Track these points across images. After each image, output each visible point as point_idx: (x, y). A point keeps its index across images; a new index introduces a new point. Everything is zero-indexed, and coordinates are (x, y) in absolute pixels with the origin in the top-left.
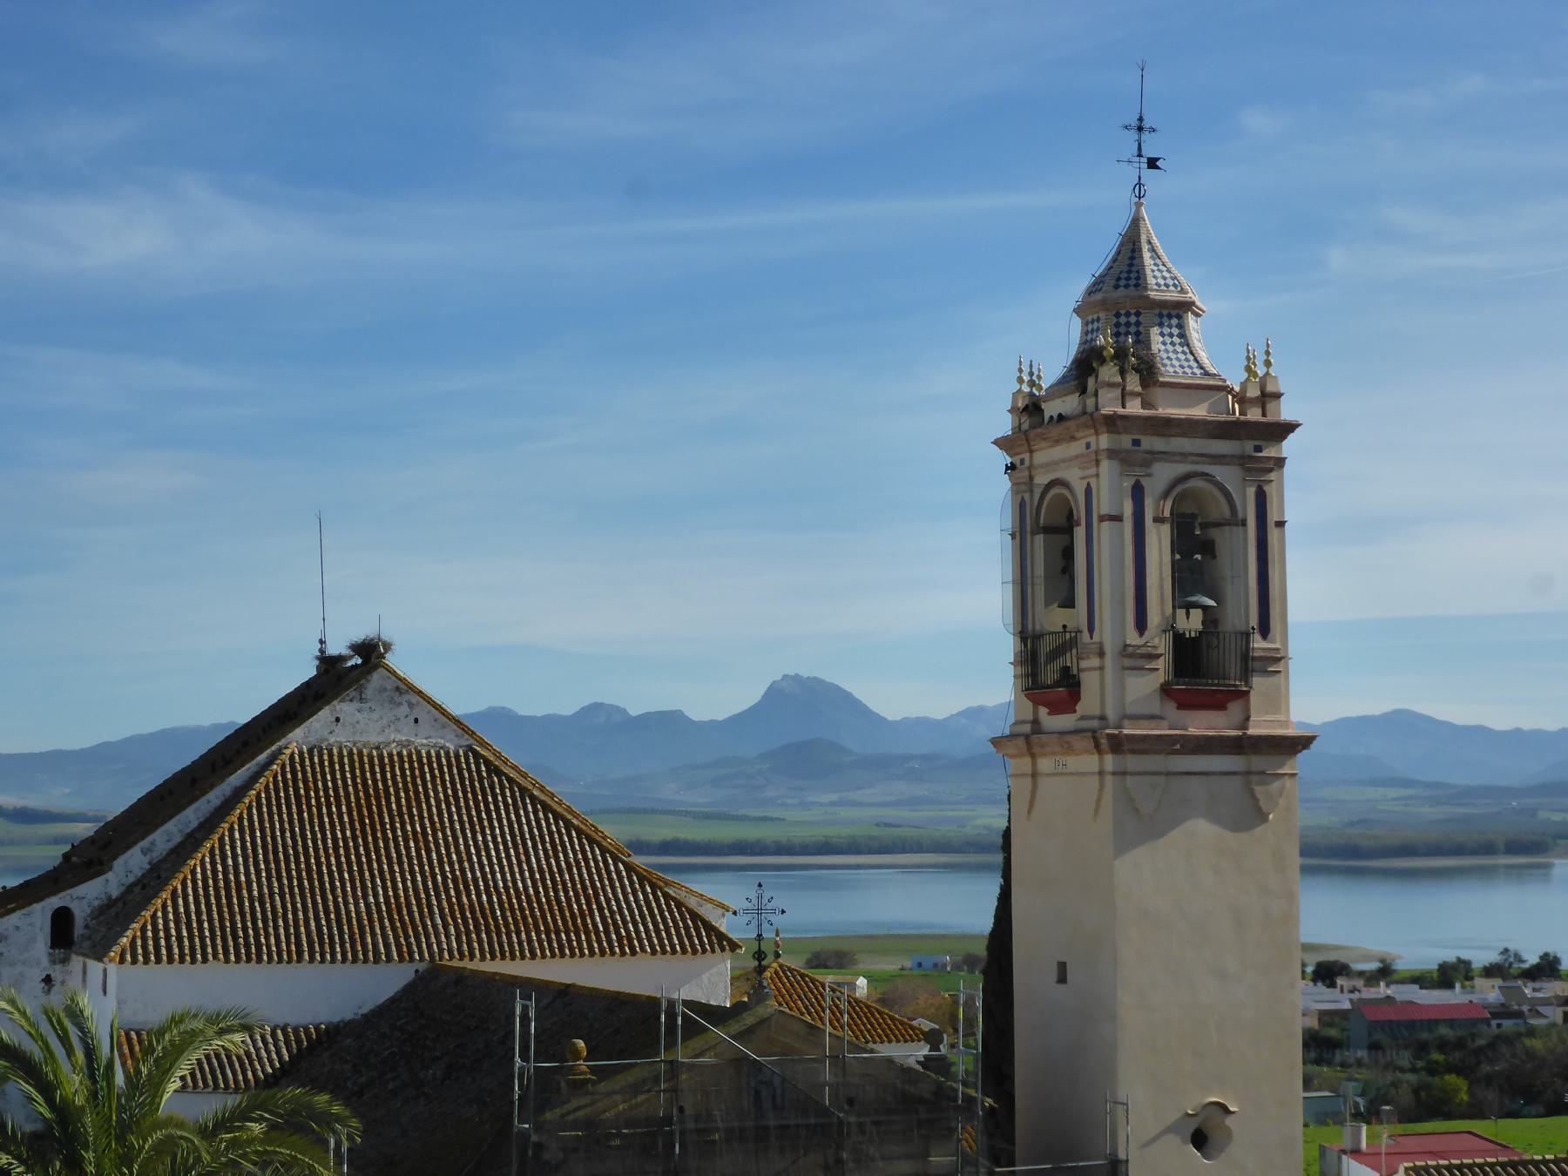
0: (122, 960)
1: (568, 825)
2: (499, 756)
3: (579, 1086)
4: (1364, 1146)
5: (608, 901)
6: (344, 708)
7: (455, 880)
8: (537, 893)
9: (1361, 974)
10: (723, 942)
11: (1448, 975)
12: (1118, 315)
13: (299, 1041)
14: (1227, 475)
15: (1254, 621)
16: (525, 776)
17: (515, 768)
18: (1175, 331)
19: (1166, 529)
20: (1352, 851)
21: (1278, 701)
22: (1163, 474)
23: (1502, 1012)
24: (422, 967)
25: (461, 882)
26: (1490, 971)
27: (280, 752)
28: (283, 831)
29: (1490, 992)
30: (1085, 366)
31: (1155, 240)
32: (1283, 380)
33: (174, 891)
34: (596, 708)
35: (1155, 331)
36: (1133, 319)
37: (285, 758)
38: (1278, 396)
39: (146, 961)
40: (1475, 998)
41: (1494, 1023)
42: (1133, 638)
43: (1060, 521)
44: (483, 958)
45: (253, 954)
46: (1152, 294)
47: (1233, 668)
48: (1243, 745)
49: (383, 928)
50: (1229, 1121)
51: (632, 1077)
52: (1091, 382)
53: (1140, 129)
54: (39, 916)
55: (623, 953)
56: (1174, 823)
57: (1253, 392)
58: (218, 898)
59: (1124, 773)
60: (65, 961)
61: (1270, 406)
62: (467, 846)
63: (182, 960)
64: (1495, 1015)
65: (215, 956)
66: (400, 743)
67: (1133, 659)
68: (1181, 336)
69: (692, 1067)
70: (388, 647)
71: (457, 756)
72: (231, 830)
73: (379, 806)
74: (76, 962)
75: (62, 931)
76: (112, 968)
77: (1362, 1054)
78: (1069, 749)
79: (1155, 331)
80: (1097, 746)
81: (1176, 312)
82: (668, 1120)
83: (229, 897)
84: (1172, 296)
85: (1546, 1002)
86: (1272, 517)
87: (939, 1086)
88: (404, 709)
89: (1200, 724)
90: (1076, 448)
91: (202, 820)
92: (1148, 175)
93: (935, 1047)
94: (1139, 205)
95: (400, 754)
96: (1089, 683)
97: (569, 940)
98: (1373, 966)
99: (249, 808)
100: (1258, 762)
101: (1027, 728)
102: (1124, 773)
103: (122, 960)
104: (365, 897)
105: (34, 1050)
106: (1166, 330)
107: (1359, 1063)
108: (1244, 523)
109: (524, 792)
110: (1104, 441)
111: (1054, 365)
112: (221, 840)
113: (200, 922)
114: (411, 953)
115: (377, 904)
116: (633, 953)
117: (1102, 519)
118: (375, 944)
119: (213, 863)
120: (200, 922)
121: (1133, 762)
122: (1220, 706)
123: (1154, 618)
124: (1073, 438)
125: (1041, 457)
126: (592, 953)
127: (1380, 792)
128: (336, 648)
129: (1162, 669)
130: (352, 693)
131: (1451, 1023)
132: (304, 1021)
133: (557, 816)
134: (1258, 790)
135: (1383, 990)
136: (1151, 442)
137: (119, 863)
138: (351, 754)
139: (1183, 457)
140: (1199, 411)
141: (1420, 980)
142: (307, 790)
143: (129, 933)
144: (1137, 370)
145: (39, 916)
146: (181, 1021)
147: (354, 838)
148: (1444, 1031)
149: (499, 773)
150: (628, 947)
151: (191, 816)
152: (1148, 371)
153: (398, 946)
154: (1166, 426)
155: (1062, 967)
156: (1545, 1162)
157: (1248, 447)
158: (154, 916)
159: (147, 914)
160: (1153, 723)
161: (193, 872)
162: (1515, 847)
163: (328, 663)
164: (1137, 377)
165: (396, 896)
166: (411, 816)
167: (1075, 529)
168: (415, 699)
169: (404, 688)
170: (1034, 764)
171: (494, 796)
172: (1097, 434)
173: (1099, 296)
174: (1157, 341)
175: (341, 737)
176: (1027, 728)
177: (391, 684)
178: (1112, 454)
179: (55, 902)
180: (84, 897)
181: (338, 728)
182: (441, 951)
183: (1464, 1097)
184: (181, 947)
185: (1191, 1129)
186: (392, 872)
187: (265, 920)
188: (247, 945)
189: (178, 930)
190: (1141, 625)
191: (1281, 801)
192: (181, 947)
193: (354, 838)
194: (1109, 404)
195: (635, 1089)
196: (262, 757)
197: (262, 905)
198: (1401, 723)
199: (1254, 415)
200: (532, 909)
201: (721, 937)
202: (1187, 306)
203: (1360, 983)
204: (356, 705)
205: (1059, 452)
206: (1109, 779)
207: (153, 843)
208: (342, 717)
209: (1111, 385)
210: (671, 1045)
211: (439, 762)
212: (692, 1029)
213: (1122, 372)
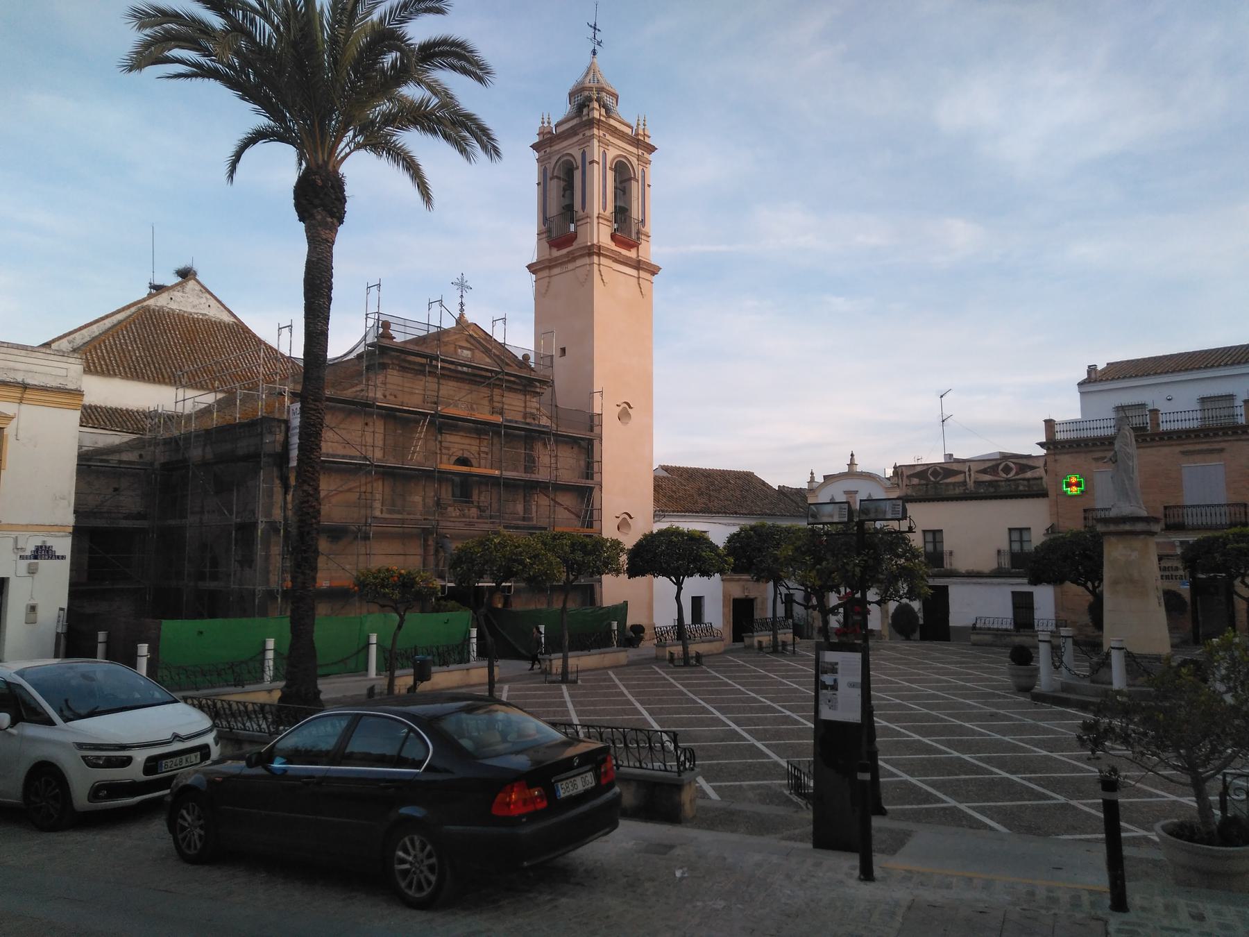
88: (204, 300)
91: (101, 332)
92: (597, 47)
146: (463, 140)
167: (575, 171)
175: (174, 306)
190: (605, 209)
204: (180, 294)
207: (74, 339)
208: (173, 297)
211: (227, 326)
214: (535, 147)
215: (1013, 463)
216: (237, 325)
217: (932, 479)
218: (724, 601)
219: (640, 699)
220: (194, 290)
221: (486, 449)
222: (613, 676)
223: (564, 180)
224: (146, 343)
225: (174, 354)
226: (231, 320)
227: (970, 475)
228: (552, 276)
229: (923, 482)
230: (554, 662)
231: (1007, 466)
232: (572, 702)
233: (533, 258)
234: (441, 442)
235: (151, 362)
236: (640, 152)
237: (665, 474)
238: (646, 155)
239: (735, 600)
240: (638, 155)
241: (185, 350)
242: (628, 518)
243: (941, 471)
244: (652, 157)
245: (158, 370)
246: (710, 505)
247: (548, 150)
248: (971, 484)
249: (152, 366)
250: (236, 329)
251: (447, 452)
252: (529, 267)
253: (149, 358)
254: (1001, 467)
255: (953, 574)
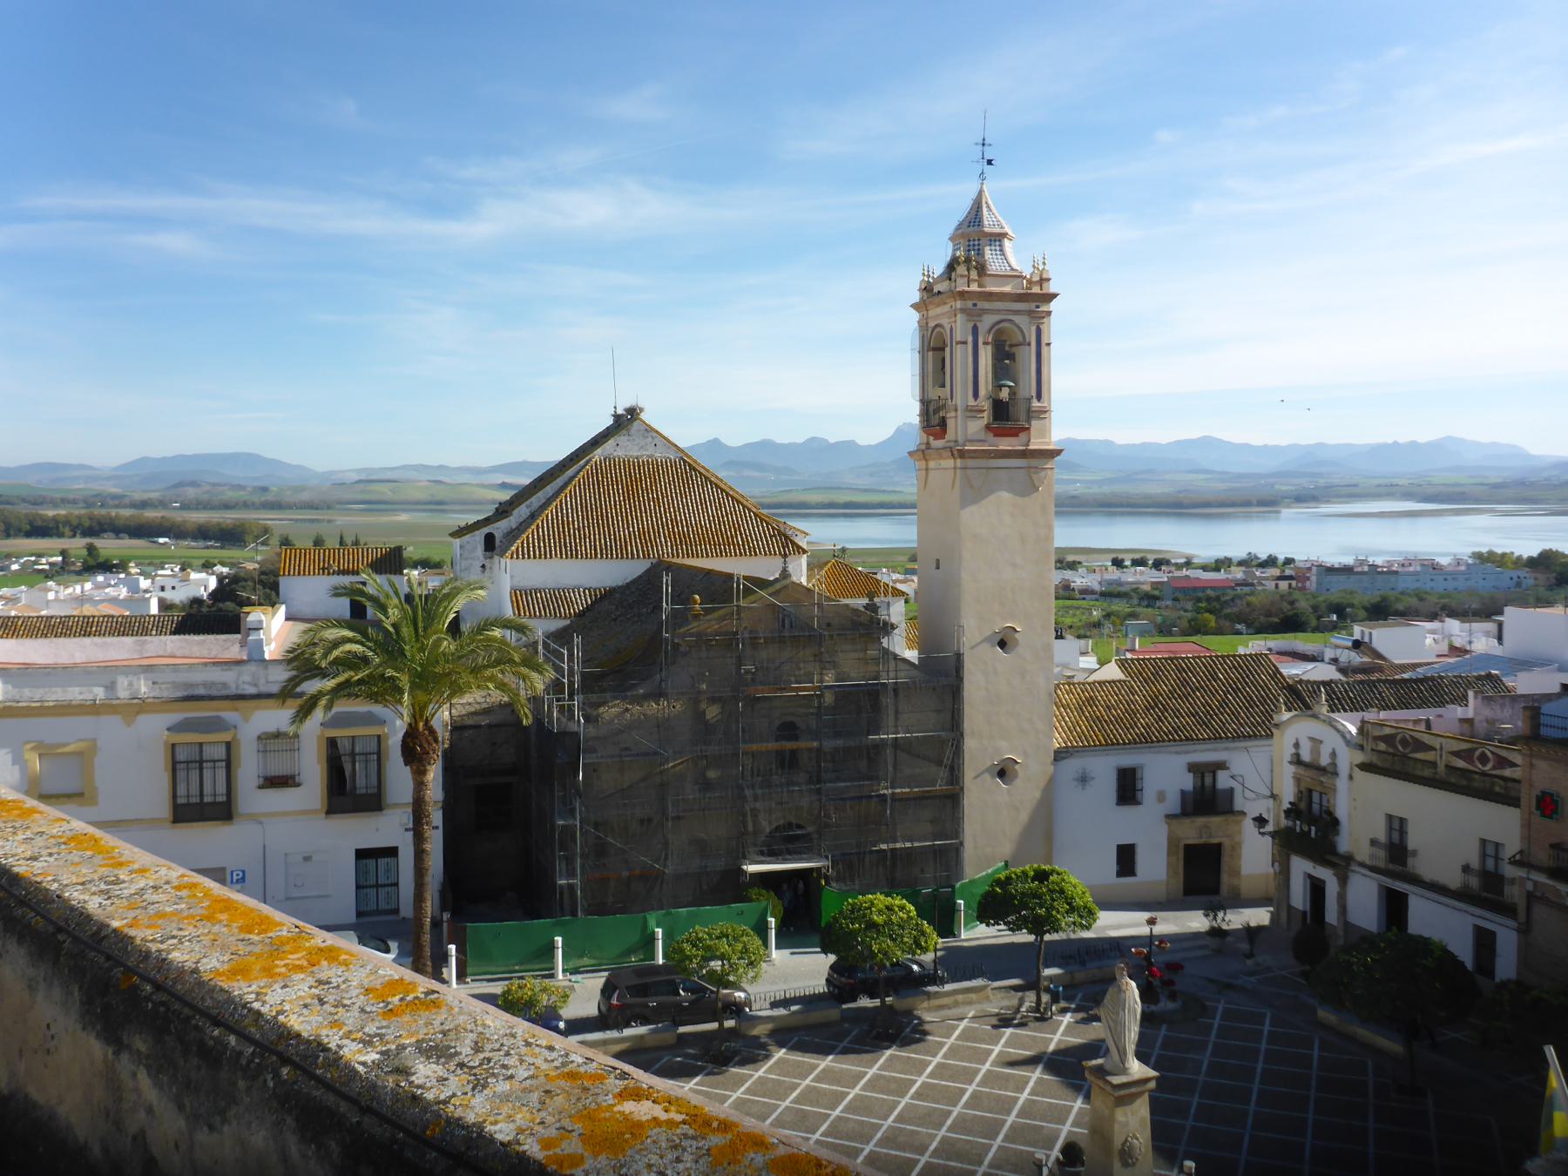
0: (512, 558)
1: (727, 494)
2: (695, 462)
3: (696, 617)
4: (1137, 647)
5: (745, 530)
6: (622, 439)
7: (672, 521)
8: (711, 527)
9: (1176, 564)
10: (805, 552)
11: (1220, 564)
12: (969, 241)
13: (596, 595)
14: (1021, 320)
15: (1034, 393)
16: (708, 471)
17: (703, 467)
18: (998, 248)
19: (989, 348)
20: (1109, 505)
21: (1045, 432)
22: (987, 321)
23: (1244, 583)
24: (654, 561)
25: (675, 522)
26: (1241, 563)
27: (590, 460)
28: (590, 497)
29: (1238, 574)
30: (951, 267)
31: (990, 202)
32: (1052, 271)
33: (538, 525)
34: (813, 439)
35: (987, 248)
36: (976, 243)
37: (593, 462)
38: (1049, 280)
39: (523, 558)
40: (1230, 577)
41: (1238, 588)
42: (971, 402)
43: (940, 345)
44: (683, 557)
45: (573, 554)
46: (986, 229)
47: (1023, 416)
48: (1025, 454)
49: (636, 543)
50: (1017, 635)
51: (721, 612)
52: (953, 274)
53: (983, 145)
54: (479, 536)
55: (751, 555)
56: (991, 492)
57: (1036, 278)
58: (558, 528)
59: (966, 468)
60: (491, 557)
61: (1045, 285)
62: (678, 504)
63: (540, 557)
64: (1237, 585)
65: (556, 555)
66: (649, 456)
67: (973, 412)
68: (1001, 250)
69: (749, 608)
70: (642, 410)
71: (675, 462)
72: (566, 497)
73: (637, 486)
74: (496, 558)
75: (490, 543)
76: (508, 560)
77: (1169, 603)
78: (941, 457)
79: (987, 248)
80: (953, 455)
81: (998, 238)
82: (737, 633)
83: (563, 528)
84: (997, 230)
85: (1266, 579)
86: (1044, 340)
87: (872, 617)
89: (1005, 444)
90: (946, 308)
93: (871, 599)
94: (982, 184)
95: (648, 461)
96: (950, 423)
97: (725, 549)
98: (1182, 561)
99: (575, 486)
100: (1034, 462)
101: (924, 447)
102: (966, 468)
103: (512, 558)
104: (628, 528)
105: (382, 599)
106: (993, 248)
107: (1167, 607)
108: (1029, 344)
109: (706, 479)
110: (959, 304)
111: (939, 269)
112: (561, 501)
113: (549, 540)
114: (649, 555)
115: (634, 532)
116: (756, 555)
117: (957, 343)
118: (632, 550)
119: (557, 512)
120: (549, 540)
121: (971, 463)
122: (1016, 435)
123: (982, 392)
124: (945, 303)
125: (931, 313)
126: (736, 555)
127: (1194, 476)
128: (620, 411)
129: (986, 417)
130: (624, 432)
131: (1213, 588)
132: (599, 586)
133: (722, 490)
134: (1035, 477)
135: (1185, 572)
136: (982, 305)
137: (515, 512)
138: (624, 461)
139: (998, 311)
140: (1007, 289)
141: (1205, 568)
142: (603, 477)
143: (516, 545)
144: (976, 268)
145: (479, 536)
147: (624, 501)
148: (1209, 592)
149: (695, 470)
150: (753, 552)
151: (549, 490)
152: (982, 269)
153: (643, 551)
154: (990, 296)
155: (938, 561)
156: (1188, 658)
157: (1032, 306)
158: (528, 537)
159: (525, 536)
160: (981, 443)
161: (547, 516)
162: (1262, 503)
163: (617, 417)
164: (976, 272)
165: (643, 528)
166: (652, 490)
168: (654, 434)
169: (649, 429)
170: (927, 464)
171: (692, 480)
172: (955, 301)
173: (960, 231)
174: (988, 253)
175: (620, 453)
176: (924, 447)
177: (644, 427)
178: (963, 310)
179: (486, 530)
180: (500, 528)
181: (618, 449)
182: (663, 554)
183: (1213, 624)
184: (540, 551)
185: (998, 640)
186: (642, 516)
187: (580, 539)
188: (571, 550)
189: (539, 543)
190: (976, 395)
191: (1045, 482)
192: (540, 551)
193: (624, 501)
194: (961, 286)
195: (723, 618)
196: (582, 462)
197: (579, 531)
198: (1207, 442)
199: (1036, 290)
200: (708, 534)
201: (799, 547)
202: (1004, 235)
203: (1173, 569)
204: (626, 438)
205: (939, 310)
206: (958, 471)
209: (962, 276)
210: (738, 600)
212: (747, 591)
213: (968, 270)
215: (1492, 752)
217: (1400, 748)
220: (639, 430)
227: (1441, 756)
229: (1391, 750)
231: (1483, 754)
239: (1188, 848)
243: (1411, 741)
248: (1441, 768)
254: (1477, 753)
255: (1416, 880)
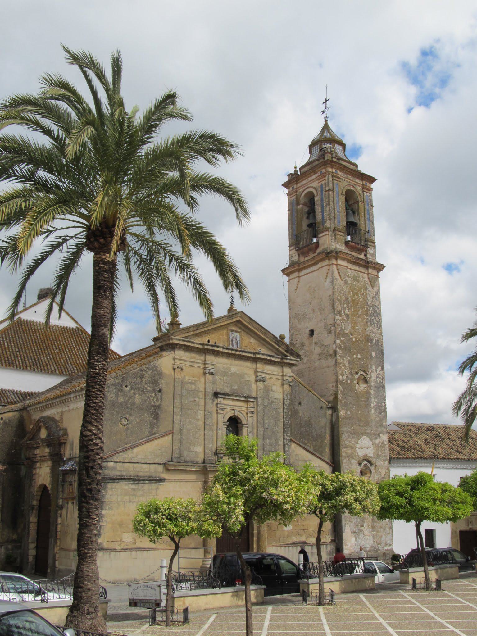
211: (71, 330)
214: (286, 185)
216: (78, 328)
218: (452, 533)
219: (390, 623)
221: (252, 410)
222: (364, 599)
223: (308, 207)
224: (17, 342)
225: (35, 350)
226: (73, 325)
228: (301, 276)
230: (311, 586)
232: (329, 624)
233: (286, 263)
234: (217, 404)
235: (19, 355)
236: (364, 183)
237: (397, 428)
238: (368, 184)
239: (461, 532)
240: (363, 185)
241: (42, 347)
242: (369, 465)
244: (373, 186)
245: (23, 361)
246: (436, 453)
247: (295, 186)
249: (19, 358)
250: (77, 332)
251: (221, 412)
252: (283, 271)
253: (18, 353)
